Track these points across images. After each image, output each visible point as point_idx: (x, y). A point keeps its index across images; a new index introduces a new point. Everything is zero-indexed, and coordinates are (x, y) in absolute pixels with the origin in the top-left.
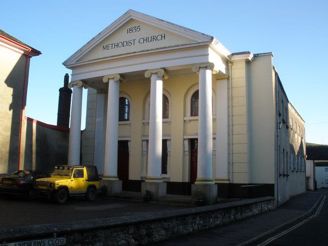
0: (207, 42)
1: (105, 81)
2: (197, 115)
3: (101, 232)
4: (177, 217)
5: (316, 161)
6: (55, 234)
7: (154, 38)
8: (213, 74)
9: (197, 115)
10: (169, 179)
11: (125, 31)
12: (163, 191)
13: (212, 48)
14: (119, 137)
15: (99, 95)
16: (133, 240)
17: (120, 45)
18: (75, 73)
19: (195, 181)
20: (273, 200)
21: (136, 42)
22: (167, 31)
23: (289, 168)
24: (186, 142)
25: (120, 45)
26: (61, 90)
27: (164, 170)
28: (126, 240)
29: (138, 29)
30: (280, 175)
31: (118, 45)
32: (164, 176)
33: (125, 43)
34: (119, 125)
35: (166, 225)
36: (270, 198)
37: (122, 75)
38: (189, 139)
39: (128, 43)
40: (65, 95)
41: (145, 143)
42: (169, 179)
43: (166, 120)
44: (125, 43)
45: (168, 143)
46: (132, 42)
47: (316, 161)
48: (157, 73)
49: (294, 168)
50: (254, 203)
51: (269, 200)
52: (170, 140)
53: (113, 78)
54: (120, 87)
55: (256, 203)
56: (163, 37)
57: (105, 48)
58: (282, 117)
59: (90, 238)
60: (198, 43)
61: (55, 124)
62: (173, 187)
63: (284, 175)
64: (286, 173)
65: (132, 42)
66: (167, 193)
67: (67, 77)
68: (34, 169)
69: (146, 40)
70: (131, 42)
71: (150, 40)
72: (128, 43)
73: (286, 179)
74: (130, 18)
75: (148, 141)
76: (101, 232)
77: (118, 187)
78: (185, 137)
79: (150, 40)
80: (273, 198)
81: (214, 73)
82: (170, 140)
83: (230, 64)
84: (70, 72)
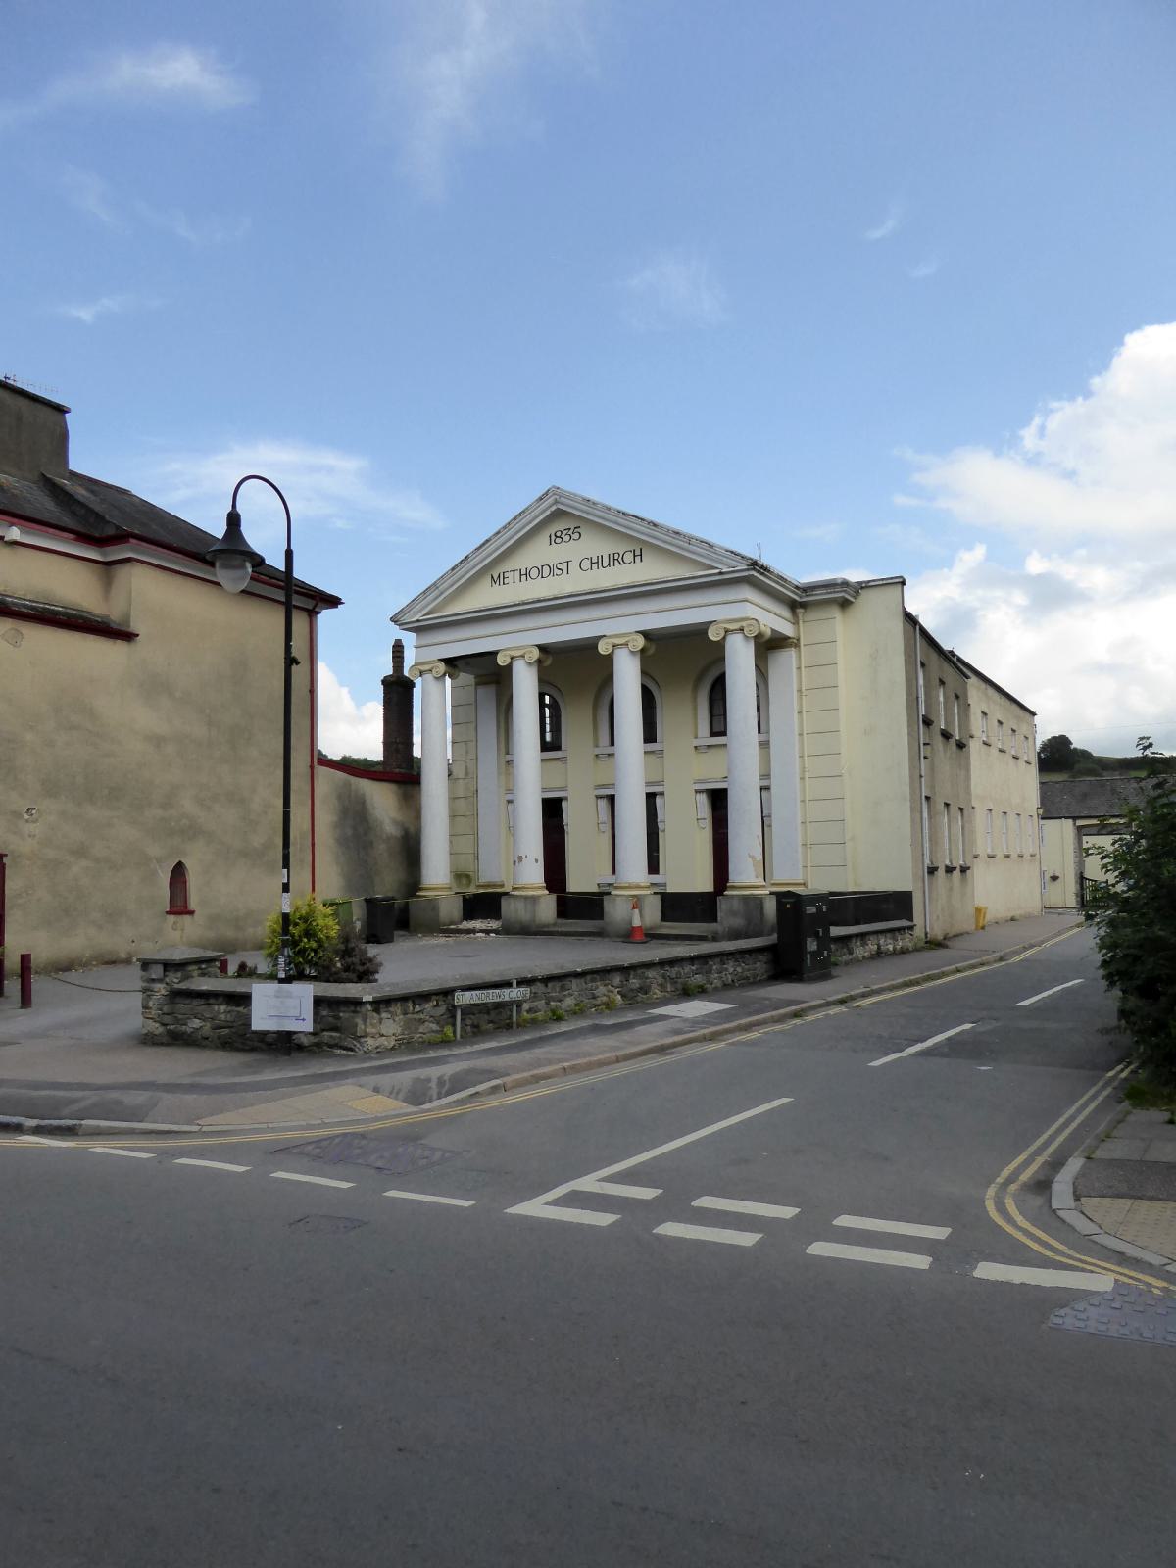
1: (502, 661)
2: (724, 733)
4: (692, 960)
5: (1080, 823)
9: (724, 733)
10: (665, 885)
11: (543, 539)
12: (651, 914)
14: (544, 790)
15: (481, 690)
16: (619, 997)
17: (534, 573)
18: (424, 642)
19: (725, 888)
20: (911, 928)
21: (574, 566)
25: (534, 573)
26: (387, 683)
27: (653, 867)
29: (575, 533)
32: (655, 878)
33: (546, 570)
34: (542, 760)
35: (673, 972)
36: (904, 923)
37: (542, 648)
40: (398, 694)
41: (603, 804)
42: (665, 885)
43: (651, 746)
44: (546, 570)
45: (658, 800)
46: (564, 567)
47: (1080, 823)
50: (857, 935)
52: (662, 794)
53: (523, 656)
55: (863, 936)
56: (638, 555)
60: (721, 574)
61: (831, 927)
62: (676, 906)
64: (959, 862)
65: (564, 567)
66: (664, 918)
67: (398, 650)
68: (1113, 890)
69: (597, 562)
70: (559, 572)
71: (605, 564)
74: (553, 508)
75: (612, 799)
77: (547, 909)
78: (698, 787)
79: (605, 564)
80: (909, 924)
82: (662, 794)
84: (409, 640)
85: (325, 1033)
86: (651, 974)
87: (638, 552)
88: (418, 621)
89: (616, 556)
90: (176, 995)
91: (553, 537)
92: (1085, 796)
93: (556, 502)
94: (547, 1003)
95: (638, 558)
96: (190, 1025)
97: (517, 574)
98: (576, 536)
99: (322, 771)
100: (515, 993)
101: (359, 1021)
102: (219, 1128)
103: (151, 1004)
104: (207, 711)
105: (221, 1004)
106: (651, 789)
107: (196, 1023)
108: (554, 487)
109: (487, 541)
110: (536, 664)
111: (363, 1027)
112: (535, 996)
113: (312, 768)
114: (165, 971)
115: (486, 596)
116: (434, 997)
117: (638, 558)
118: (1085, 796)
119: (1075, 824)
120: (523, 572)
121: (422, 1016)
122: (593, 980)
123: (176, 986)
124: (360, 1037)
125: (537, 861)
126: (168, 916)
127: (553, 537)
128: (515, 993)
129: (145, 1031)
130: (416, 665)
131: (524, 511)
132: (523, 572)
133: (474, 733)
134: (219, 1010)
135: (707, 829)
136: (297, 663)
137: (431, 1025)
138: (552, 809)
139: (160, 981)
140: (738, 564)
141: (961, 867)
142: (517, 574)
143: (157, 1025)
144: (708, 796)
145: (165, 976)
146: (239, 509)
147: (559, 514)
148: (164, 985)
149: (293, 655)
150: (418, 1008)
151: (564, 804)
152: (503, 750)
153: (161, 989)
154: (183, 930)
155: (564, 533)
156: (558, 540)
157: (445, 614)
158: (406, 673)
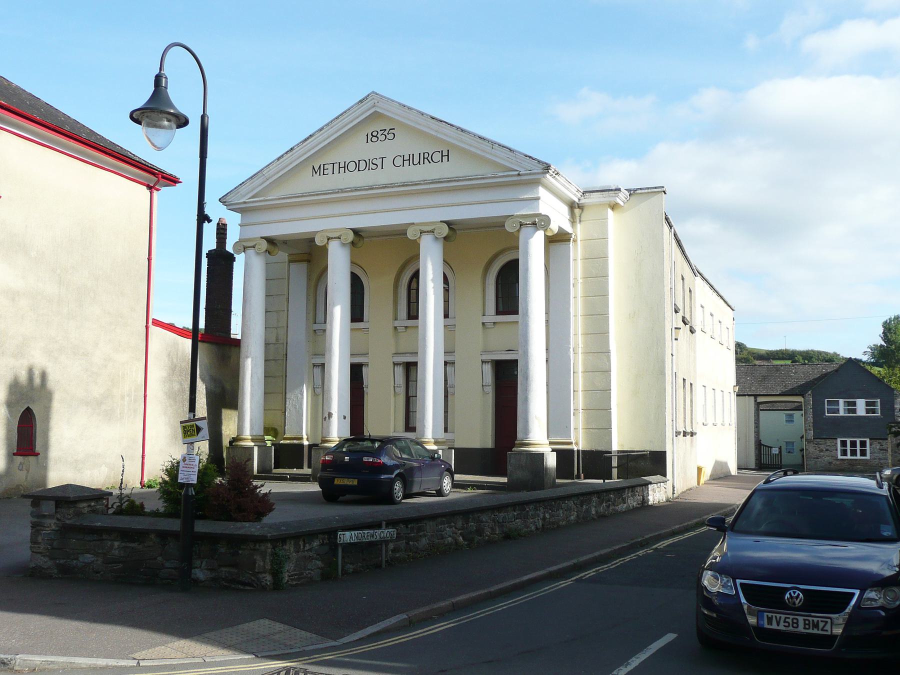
0: (538, 173)
2: (416, 317)
3: (426, 523)
4: (514, 505)
5: (760, 399)
6: (384, 523)
7: (426, 158)
8: (545, 235)
13: (547, 187)
16: (461, 538)
17: (352, 166)
21: (388, 162)
22: (455, 146)
23: (186, 466)
24: (488, 369)
25: (352, 166)
28: (453, 538)
29: (389, 133)
30: (678, 433)
31: (346, 167)
32: (449, 436)
33: (362, 165)
34: (352, 329)
37: (356, 232)
38: (492, 361)
39: (370, 164)
43: (449, 321)
44: (362, 165)
46: (379, 162)
47: (760, 399)
48: (432, 231)
49: (197, 453)
50: (628, 487)
51: (517, 354)
54: (352, 255)
56: (445, 156)
57: (319, 170)
58: (680, 314)
59: (415, 531)
63: (685, 434)
64: (689, 430)
65: (379, 162)
69: (409, 160)
71: (416, 161)
72: (370, 164)
73: (688, 443)
76: (426, 523)
78: (485, 357)
79: (416, 161)
81: (549, 234)
83: (577, 211)
85: (224, 569)
86: (484, 517)
87: (445, 153)
88: (245, 203)
89: (426, 155)
90: (65, 530)
91: (370, 136)
92: (764, 378)
93: (374, 106)
94: (407, 543)
95: (445, 158)
96: (81, 559)
97: (336, 166)
98: (390, 136)
99: (153, 329)
100: (385, 533)
101: (258, 557)
102: (168, 662)
103: (40, 539)
104: (59, 271)
105: (115, 541)
106: (357, 360)
107: (88, 558)
108: (373, 92)
109: (311, 136)
110: (349, 245)
111: (262, 564)
112: (399, 537)
113: (147, 327)
114: (57, 507)
115: (308, 183)
116: (320, 536)
117: (445, 158)
118: (764, 378)
119: (756, 401)
120: (342, 165)
121: (311, 554)
122: (442, 523)
123: (68, 522)
124: (258, 573)
125: (345, 418)
126: (14, 457)
127: (370, 136)
128: (385, 533)
129: (32, 565)
130: (240, 241)
131: (345, 112)
132: (342, 165)
133: (286, 303)
134: (112, 546)
135: (491, 394)
136: (210, 221)
137: (318, 562)
138: (356, 372)
139: (50, 517)
140: (534, 167)
141: (684, 431)
142: (336, 166)
143: (46, 559)
144: (492, 367)
145: (56, 512)
146: (166, 71)
147: (376, 116)
148: (54, 521)
149: (206, 213)
150: (308, 547)
151: (364, 369)
152: (311, 321)
153: (51, 524)
154: (28, 471)
155: (380, 133)
156: (374, 139)
157: (270, 198)
158: (229, 248)
